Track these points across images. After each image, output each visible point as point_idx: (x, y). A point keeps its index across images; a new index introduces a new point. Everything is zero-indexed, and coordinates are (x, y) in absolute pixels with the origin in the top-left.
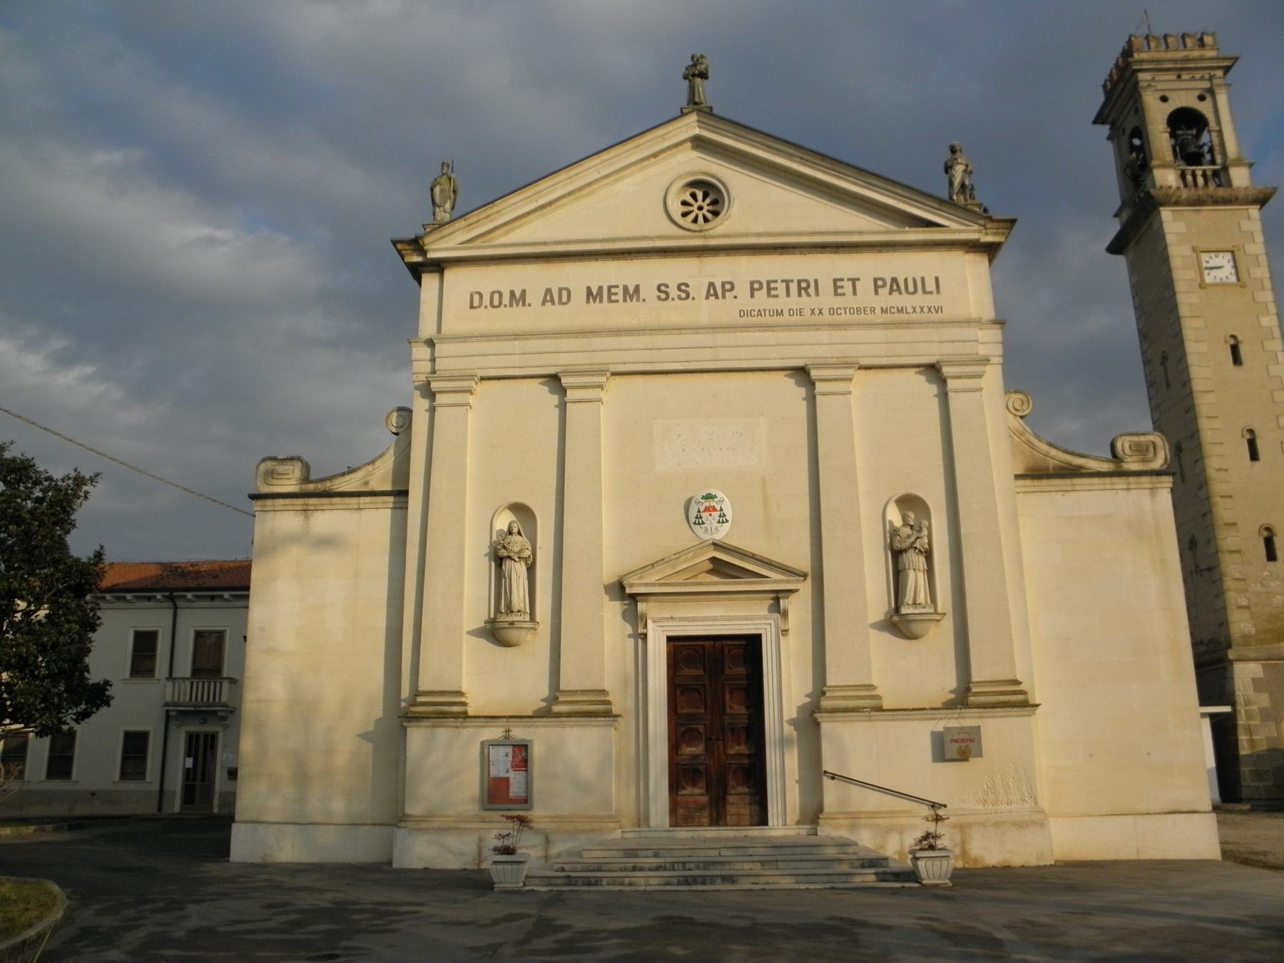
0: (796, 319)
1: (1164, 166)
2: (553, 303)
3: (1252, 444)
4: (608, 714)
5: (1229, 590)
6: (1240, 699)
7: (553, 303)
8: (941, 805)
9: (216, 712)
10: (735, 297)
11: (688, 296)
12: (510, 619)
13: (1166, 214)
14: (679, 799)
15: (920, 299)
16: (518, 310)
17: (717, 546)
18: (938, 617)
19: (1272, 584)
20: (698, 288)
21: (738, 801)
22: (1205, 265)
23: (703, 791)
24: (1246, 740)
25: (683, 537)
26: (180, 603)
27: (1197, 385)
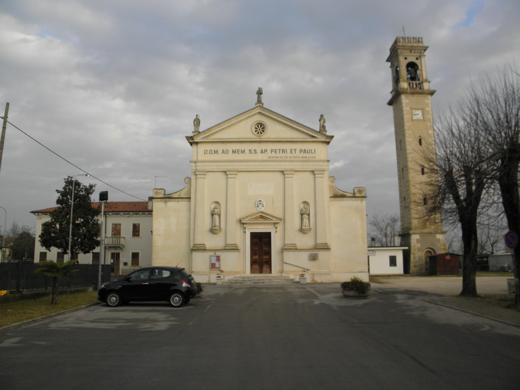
0: (281, 159)
1: (404, 81)
2: (224, 153)
4: (237, 249)
7: (224, 153)
8: (307, 270)
9: (120, 247)
10: (267, 153)
11: (256, 153)
12: (215, 228)
13: (403, 97)
14: (252, 268)
15: (310, 155)
16: (216, 155)
17: (262, 212)
18: (310, 229)
20: (259, 150)
21: (265, 268)
23: (258, 266)
25: (254, 210)
26: (107, 216)
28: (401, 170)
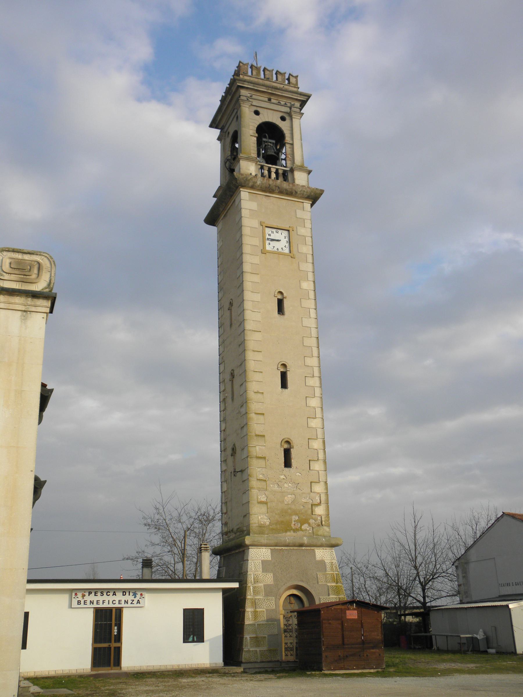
1: (249, 159)
3: (284, 376)
6: (251, 578)
13: (244, 194)
19: (286, 485)
22: (267, 237)
27: (249, 326)
28: (228, 377)
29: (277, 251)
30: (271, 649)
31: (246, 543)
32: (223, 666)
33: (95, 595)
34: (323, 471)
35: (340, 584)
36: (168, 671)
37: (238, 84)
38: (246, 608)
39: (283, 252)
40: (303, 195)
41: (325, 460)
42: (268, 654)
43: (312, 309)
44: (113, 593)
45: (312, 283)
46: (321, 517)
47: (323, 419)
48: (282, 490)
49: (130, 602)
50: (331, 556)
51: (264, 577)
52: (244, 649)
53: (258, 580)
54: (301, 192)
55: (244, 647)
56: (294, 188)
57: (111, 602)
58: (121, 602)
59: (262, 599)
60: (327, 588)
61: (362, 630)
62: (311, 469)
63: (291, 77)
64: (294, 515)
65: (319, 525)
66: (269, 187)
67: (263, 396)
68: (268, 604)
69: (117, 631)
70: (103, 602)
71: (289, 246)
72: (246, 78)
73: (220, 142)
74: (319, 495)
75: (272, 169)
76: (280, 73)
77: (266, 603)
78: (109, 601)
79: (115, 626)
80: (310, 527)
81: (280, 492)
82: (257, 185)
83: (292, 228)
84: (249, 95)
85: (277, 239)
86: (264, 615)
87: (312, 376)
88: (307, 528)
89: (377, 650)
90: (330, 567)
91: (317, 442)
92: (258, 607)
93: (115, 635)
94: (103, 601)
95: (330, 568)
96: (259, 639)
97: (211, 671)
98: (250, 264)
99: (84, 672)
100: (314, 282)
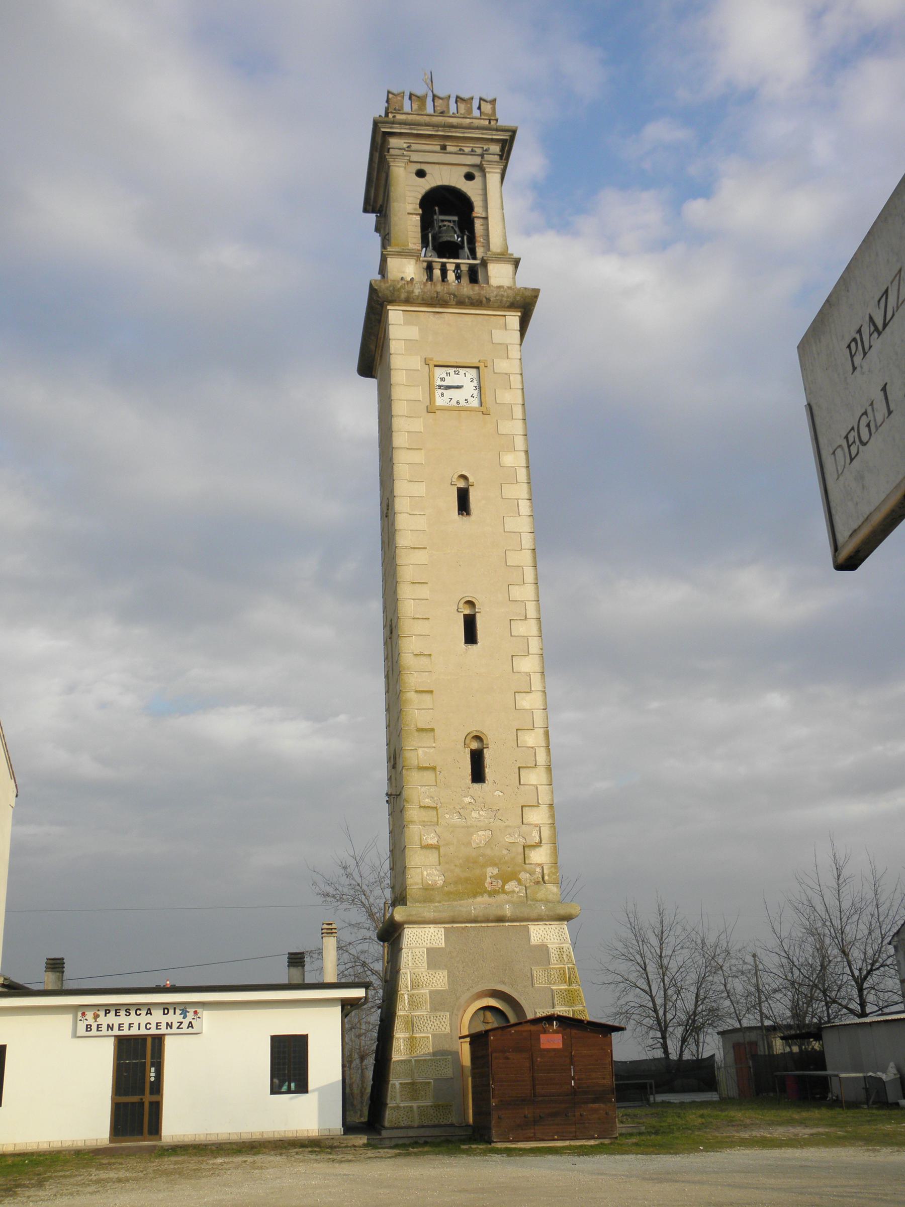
1: (405, 254)
5: (412, 822)
19: (474, 814)
22: (439, 383)
24: (404, 1039)
29: (457, 405)
30: (440, 1103)
31: (395, 918)
32: (342, 1133)
33: (116, 1015)
34: (544, 785)
35: (574, 987)
36: (230, 1143)
37: (383, 130)
38: (395, 1033)
39: (468, 405)
40: (501, 302)
41: (550, 766)
42: (434, 1112)
43: (522, 499)
44: (147, 1012)
45: (523, 455)
46: (543, 867)
47: (545, 693)
48: (467, 823)
49: (175, 1025)
50: (559, 936)
51: (430, 977)
52: (390, 1104)
53: (419, 982)
54: (497, 298)
55: (388, 1101)
56: (483, 292)
57: (143, 1026)
58: (123, 1027)
59: (425, 1016)
60: (550, 993)
61: (571, 1069)
62: (521, 783)
63: (483, 103)
64: (490, 866)
65: (538, 883)
66: (437, 297)
67: (431, 659)
68: (436, 1025)
69: (151, 1074)
70: (130, 1026)
71: (479, 395)
72: (399, 117)
73: (379, 234)
74: (538, 828)
75: (448, 265)
76: (463, 100)
77: (433, 1022)
78: (139, 1024)
79: (152, 1065)
80: (520, 887)
81: (463, 827)
82: (416, 296)
83: (485, 362)
84: (405, 146)
85: (456, 384)
86: (428, 1044)
87: (524, 618)
88: (515, 889)
89: (602, 1106)
90: (557, 956)
91: (533, 735)
92: (416, 1030)
93: (151, 1082)
94: (130, 1024)
95: (558, 958)
96: (417, 1087)
97: (307, 1142)
98: (406, 433)
99: (98, 1144)
100: (526, 452)
